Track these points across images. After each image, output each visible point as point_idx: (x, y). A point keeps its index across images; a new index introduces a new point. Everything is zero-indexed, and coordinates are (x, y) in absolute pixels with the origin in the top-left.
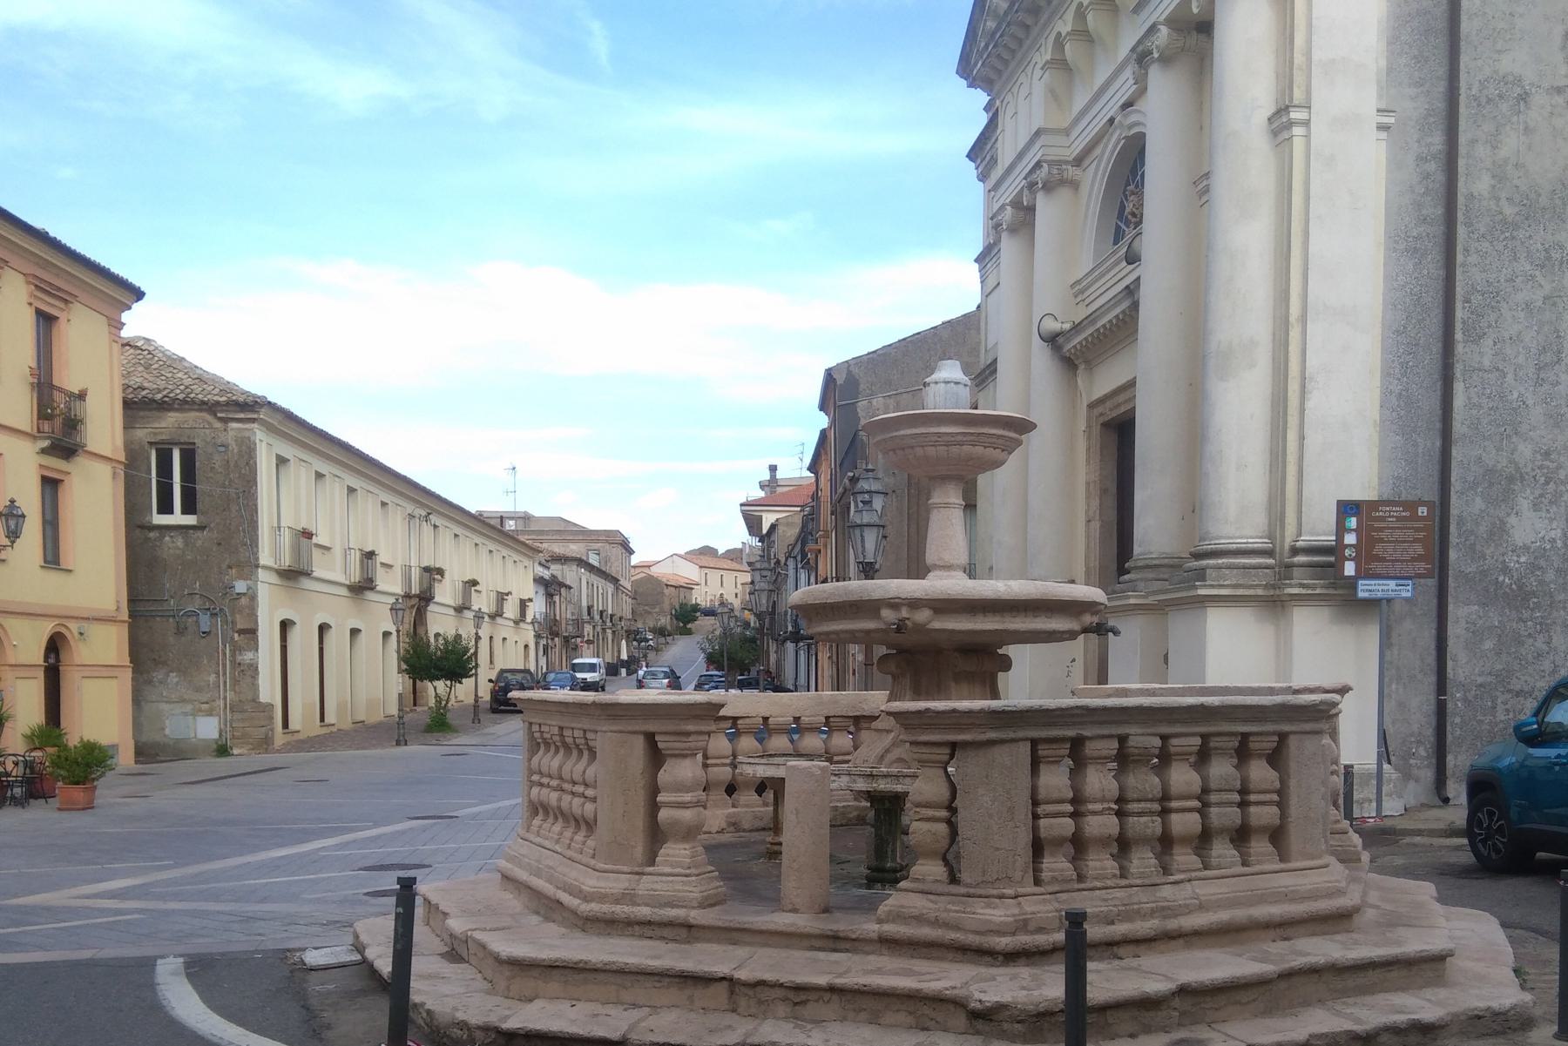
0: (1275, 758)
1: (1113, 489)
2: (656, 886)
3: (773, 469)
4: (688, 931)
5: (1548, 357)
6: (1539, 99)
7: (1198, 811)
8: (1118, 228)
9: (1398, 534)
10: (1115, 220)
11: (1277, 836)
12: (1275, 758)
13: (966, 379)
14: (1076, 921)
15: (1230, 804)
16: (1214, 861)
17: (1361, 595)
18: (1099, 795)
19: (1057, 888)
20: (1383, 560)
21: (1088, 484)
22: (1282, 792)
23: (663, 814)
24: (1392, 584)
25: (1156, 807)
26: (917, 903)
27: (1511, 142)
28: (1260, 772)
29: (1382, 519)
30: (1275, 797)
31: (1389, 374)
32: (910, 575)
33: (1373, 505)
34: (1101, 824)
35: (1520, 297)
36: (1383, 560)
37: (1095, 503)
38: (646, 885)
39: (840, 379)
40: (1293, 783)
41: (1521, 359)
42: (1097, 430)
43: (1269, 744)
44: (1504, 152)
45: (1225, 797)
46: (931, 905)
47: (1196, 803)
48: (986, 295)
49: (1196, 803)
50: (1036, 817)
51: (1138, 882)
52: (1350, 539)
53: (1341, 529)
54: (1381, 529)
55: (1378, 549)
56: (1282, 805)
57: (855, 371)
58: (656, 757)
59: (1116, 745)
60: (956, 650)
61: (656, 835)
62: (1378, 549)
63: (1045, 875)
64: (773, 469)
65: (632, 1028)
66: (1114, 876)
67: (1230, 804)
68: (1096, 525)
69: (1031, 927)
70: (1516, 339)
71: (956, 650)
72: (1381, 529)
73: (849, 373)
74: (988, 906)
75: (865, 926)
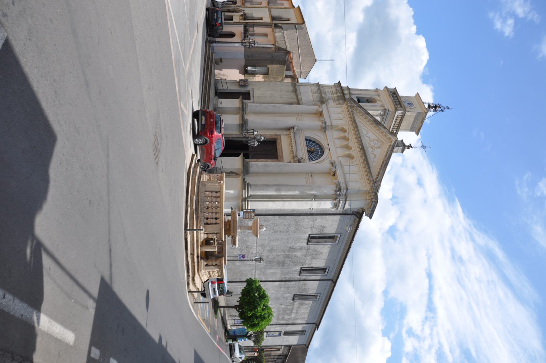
26: (203, 264)
27: (307, 221)
42: (275, 137)
53: (250, 210)
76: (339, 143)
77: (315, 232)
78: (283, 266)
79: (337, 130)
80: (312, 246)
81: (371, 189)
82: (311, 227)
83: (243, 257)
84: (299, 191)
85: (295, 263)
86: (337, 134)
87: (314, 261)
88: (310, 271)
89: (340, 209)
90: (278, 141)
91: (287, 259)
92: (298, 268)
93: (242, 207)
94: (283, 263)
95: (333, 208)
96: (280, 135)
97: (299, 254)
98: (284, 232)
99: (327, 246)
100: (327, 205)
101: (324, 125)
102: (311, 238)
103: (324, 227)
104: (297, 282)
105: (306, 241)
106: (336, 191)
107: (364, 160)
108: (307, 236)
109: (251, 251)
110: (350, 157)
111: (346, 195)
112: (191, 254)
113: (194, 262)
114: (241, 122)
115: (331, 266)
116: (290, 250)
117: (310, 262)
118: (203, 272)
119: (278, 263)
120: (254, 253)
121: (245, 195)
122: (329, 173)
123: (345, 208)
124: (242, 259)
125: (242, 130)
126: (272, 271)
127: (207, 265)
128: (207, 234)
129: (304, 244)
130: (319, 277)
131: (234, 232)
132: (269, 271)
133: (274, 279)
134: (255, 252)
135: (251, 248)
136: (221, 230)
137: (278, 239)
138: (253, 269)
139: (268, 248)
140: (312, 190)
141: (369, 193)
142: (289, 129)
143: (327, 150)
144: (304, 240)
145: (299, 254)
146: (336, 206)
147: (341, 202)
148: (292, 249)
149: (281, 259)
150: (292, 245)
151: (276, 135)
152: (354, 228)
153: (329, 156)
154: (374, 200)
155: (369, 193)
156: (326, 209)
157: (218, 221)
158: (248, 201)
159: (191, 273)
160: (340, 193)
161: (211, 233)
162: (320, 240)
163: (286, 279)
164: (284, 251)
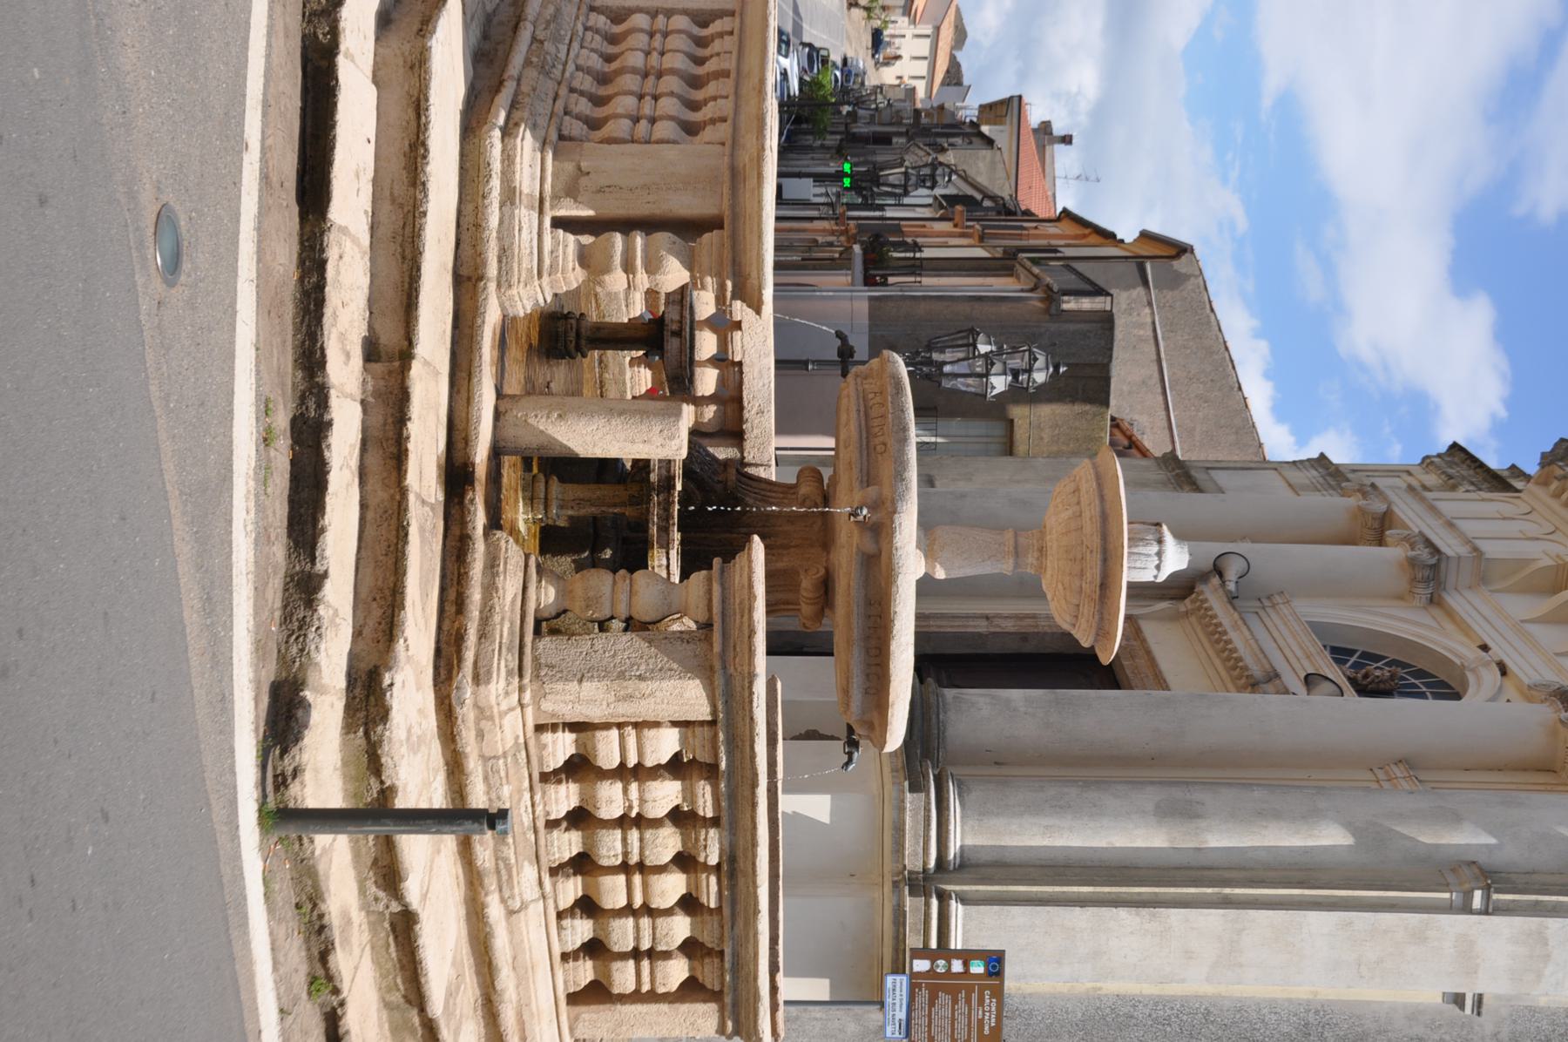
0: (691, 989)
1: (1028, 648)
3: (1067, 140)
4: (466, 281)
7: (629, 905)
8: (1351, 652)
9: (961, 1022)
10: (1361, 649)
11: (597, 993)
12: (691, 989)
13: (1162, 578)
14: (494, 819)
15: (637, 938)
16: (567, 922)
17: (890, 979)
18: (648, 796)
19: (533, 750)
20: (932, 1004)
21: (1034, 617)
22: (653, 997)
23: (618, 239)
24: (901, 1015)
25: (637, 879)
26: (510, 586)
28: (676, 972)
29: (981, 1002)
30: (646, 988)
31: (1156, 1004)
32: (916, 409)
33: (998, 993)
34: (612, 800)
36: (932, 1004)
37: (1009, 626)
38: (526, 217)
39: (1180, 265)
40: (664, 1007)
43: (709, 978)
45: (623, 597)
46: (509, 598)
47: (646, 988)
48: (1277, 467)
49: (638, 902)
50: (620, 726)
51: (542, 842)
52: (957, 966)
53: (967, 956)
54: (968, 1001)
55: (944, 999)
56: (637, 997)
57: (1190, 285)
58: (688, 229)
59: (710, 814)
60: (827, 570)
62: (944, 999)
63: (548, 737)
64: (1067, 140)
65: (344, 230)
66: (548, 814)
67: (637, 938)
68: (982, 627)
69: (485, 725)
71: (827, 570)
72: (968, 1001)
73: (1187, 277)
74: (509, 673)
84: (1349, 826)
93: (899, 938)
101: (1423, 553)
112: (371, 351)
113: (398, 457)
118: (499, 690)
121: (919, 854)
127: (548, 625)
136: (739, 178)
158: (943, 898)
159: (339, 593)
161: (627, 226)
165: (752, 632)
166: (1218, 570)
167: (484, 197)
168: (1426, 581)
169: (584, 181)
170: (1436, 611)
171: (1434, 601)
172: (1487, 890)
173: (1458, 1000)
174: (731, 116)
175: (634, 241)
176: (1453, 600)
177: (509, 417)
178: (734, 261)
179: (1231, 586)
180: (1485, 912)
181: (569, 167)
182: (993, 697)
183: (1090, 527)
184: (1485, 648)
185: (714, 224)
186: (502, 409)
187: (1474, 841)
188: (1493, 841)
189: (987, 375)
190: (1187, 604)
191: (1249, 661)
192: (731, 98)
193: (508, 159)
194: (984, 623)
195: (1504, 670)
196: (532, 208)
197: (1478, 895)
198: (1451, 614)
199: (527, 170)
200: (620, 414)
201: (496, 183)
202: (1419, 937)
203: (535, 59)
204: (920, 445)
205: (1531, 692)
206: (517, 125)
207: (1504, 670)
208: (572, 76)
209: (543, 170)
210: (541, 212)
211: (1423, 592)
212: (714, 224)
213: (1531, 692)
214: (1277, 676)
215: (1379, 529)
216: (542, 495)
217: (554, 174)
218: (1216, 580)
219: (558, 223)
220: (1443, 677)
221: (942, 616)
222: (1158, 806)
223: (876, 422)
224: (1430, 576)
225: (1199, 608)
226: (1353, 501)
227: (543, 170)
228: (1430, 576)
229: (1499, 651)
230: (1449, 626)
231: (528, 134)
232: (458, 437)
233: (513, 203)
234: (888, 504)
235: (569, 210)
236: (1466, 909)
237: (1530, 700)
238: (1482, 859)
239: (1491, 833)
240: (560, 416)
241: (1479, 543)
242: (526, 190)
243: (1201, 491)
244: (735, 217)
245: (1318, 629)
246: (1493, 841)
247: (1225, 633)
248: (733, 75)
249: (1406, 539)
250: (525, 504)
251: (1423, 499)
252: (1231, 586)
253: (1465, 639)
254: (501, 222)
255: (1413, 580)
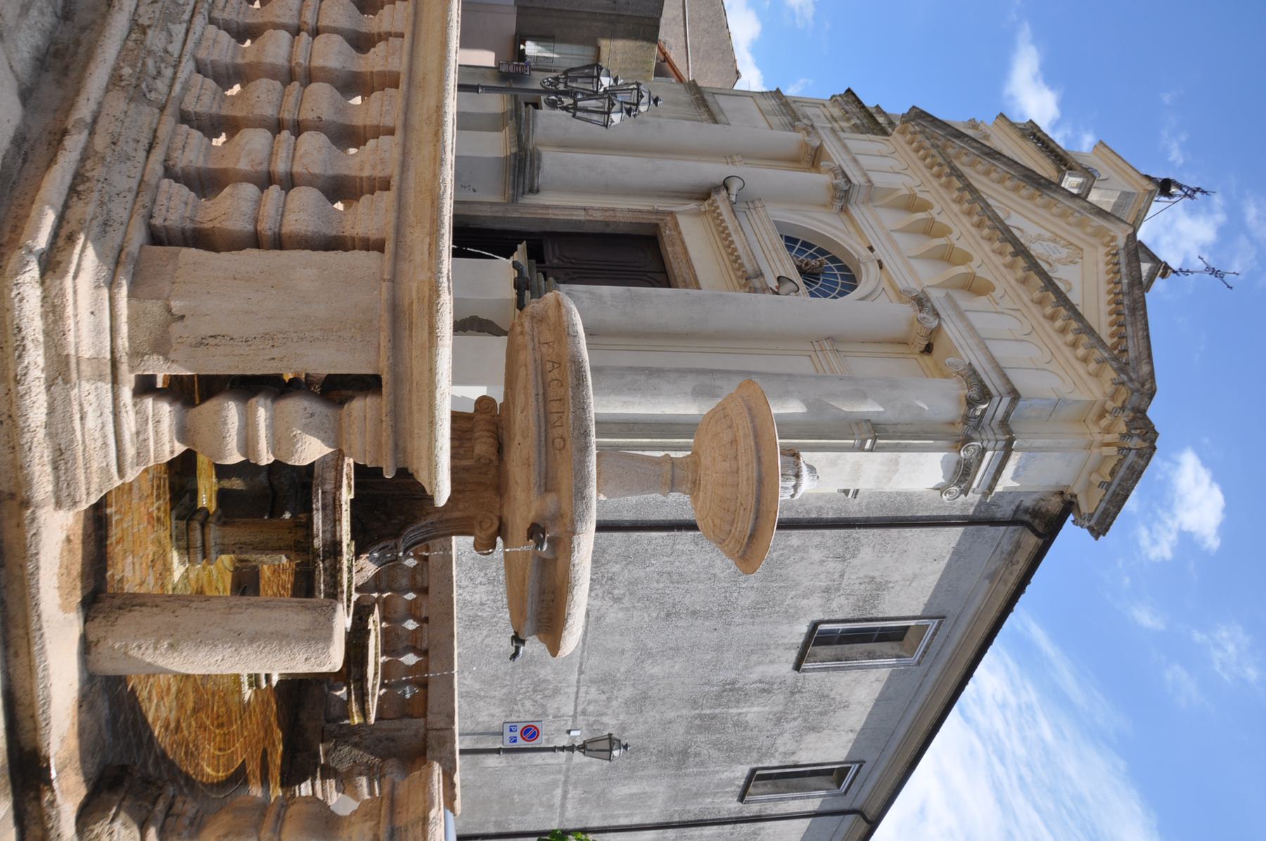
1: (609, 230)
2: (91, 422)
5: (675, 577)
6: (839, 566)
21: (614, 210)
23: (232, 411)
27: (816, 555)
35: (718, 562)
37: (598, 216)
38: (91, 397)
41: (677, 564)
42: (653, 219)
44: (812, 551)
61: (189, 392)
68: (581, 216)
70: (691, 561)
71: (500, 519)
75: (182, 303)
76: (909, 244)
77: (840, 610)
78: (680, 765)
79: (892, 206)
80: (814, 678)
81: (1113, 397)
82: (827, 590)
83: (530, 732)
84: (805, 401)
85: (732, 753)
86: (893, 219)
87: (811, 738)
88: (779, 782)
89: (969, 502)
90: (667, 233)
91: (701, 738)
92: (741, 771)
94: (684, 753)
95: (941, 489)
96: (672, 213)
97: (753, 712)
98: (708, 615)
99: (874, 674)
100: (921, 474)
101: (841, 181)
102: (823, 642)
103: (879, 587)
104: (728, 827)
105: (793, 655)
106: (971, 403)
107: (1046, 289)
108: (804, 629)
109: (552, 706)
110: (974, 287)
111: (1004, 423)
114: (514, 150)
115: (870, 758)
116: (719, 696)
117: (791, 746)
119: (665, 754)
120: (564, 720)
122: (903, 342)
123: (999, 488)
124: (521, 743)
125: (515, 186)
126: (633, 788)
128: (189, 392)
129: (784, 668)
130: (813, 804)
131: (547, 484)
132: (622, 790)
133: (636, 820)
134: (569, 709)
135: (556, 691)
137: (676, 649)
138: (554, 784)
139: (628, 692)
140: (863, 396)
141: (1101, 416)
142: (704, 194)
143: (874, 268)
144: (788, 648)
145: (753, 712)
146: (963, 474)
147: (988, 455)
148: (732, 691)
149: (677, 736)
150: (731, 675)
151: (657, 212)
152: (1006, 590)
153: (885, 284)
154: (1135, 443)
155: (1101, 416)
156: (908, 497)
157: (367, 217)
160: (984, 416)
162: (846, 649)
163: (686, 818)
164: (694, 703)
165: (439, 161)
166: (726, 185)
167: (18, 382)
168: (841, 198)
169: (176, 329)
170: (844, 216)
171: (844, 210)
172: (875, 438)
173: (846, 492)
174: (399, 124)
175: (255, 414)
176: (854, 211)
177: (103, 649)
178: (396, 447)
179: (733, 198)
180: (871, 450)
181: (155, 307)
182: (591, 293)
183: (746, 489)
184: (871, 249)
185: (369, 384)
186: (92, 637)
187: (871, 409)
188: (881, 409)
189: (608, 113)
190: (705, 206)
191: (744, 259)
192: (399, 133)
193: (53, 311)
194: (583, 213)
195: (881, 265)
196: (101, 377)
197: (869, 441)
198: (852, 220)
199: (86, 321)
200: (252, 641)
201: (35, 358)
202: (833, 464)
203: (127, 71)
204: (598, 446)
205: (901, 295)
206: (71, 239)
207: (881, 265)
208: (186, 88)
209: (113, 317)
210: (115, 381)
211: (838, 204)
212: (369, 384)
213: (901, 295)
214: (762, 274)
215: (813, 158)
216: (199, 543)
217: (132, 321)
218: (724, 193)
219: (145, 387)
220: (846, 263)
221: (557, 207)
222: (694, 390)
223: (555, 417)
224: (842, 196)
225: (714, 211)
226: (799, 136)
227: (113, 317)
228: (842, 196)
229: (879, 253)
230: (852, 230)
231: (90, 253)
232: (22, 713)
233: (66, 381)
234: (567, 521)
235: (161, 371)
236: (861, 449)
237: (900, 300)
238: (873, 419)
239: (882, 405)
240: (171, 646)
241: (871, 174)
242: (86, 353)
243: (715, 121)
244: (397, 380)
245: (778, 225)
246: (881, 409)
247: (729, 235)
248: (389, 247)
249: (831, 170)
250: (181, 555)
251: (839, 139)
252: (733, 198)
253: (859, 240)
254: (51, 411)
255: (834, 197)
